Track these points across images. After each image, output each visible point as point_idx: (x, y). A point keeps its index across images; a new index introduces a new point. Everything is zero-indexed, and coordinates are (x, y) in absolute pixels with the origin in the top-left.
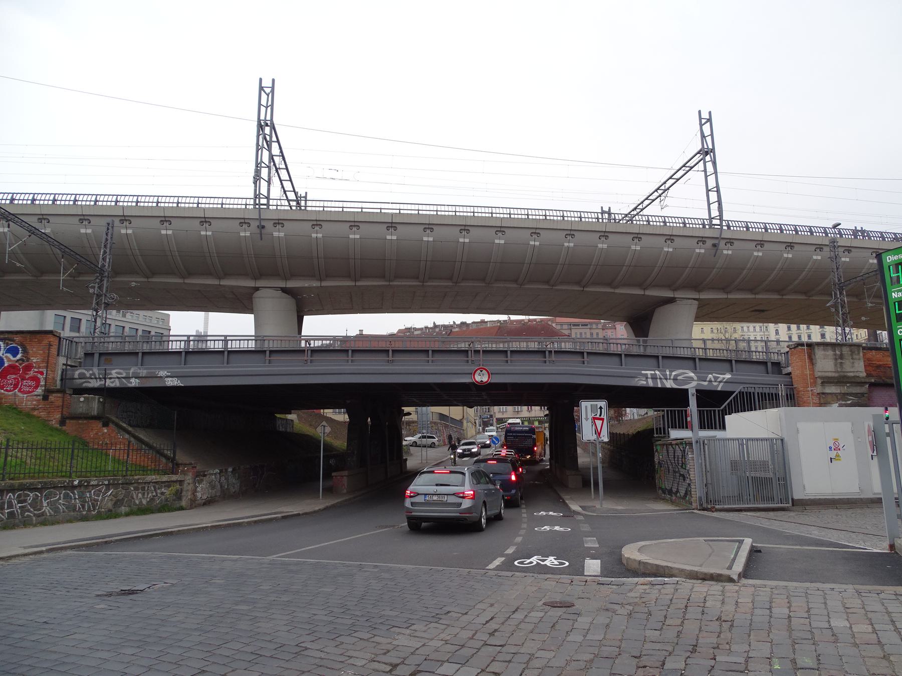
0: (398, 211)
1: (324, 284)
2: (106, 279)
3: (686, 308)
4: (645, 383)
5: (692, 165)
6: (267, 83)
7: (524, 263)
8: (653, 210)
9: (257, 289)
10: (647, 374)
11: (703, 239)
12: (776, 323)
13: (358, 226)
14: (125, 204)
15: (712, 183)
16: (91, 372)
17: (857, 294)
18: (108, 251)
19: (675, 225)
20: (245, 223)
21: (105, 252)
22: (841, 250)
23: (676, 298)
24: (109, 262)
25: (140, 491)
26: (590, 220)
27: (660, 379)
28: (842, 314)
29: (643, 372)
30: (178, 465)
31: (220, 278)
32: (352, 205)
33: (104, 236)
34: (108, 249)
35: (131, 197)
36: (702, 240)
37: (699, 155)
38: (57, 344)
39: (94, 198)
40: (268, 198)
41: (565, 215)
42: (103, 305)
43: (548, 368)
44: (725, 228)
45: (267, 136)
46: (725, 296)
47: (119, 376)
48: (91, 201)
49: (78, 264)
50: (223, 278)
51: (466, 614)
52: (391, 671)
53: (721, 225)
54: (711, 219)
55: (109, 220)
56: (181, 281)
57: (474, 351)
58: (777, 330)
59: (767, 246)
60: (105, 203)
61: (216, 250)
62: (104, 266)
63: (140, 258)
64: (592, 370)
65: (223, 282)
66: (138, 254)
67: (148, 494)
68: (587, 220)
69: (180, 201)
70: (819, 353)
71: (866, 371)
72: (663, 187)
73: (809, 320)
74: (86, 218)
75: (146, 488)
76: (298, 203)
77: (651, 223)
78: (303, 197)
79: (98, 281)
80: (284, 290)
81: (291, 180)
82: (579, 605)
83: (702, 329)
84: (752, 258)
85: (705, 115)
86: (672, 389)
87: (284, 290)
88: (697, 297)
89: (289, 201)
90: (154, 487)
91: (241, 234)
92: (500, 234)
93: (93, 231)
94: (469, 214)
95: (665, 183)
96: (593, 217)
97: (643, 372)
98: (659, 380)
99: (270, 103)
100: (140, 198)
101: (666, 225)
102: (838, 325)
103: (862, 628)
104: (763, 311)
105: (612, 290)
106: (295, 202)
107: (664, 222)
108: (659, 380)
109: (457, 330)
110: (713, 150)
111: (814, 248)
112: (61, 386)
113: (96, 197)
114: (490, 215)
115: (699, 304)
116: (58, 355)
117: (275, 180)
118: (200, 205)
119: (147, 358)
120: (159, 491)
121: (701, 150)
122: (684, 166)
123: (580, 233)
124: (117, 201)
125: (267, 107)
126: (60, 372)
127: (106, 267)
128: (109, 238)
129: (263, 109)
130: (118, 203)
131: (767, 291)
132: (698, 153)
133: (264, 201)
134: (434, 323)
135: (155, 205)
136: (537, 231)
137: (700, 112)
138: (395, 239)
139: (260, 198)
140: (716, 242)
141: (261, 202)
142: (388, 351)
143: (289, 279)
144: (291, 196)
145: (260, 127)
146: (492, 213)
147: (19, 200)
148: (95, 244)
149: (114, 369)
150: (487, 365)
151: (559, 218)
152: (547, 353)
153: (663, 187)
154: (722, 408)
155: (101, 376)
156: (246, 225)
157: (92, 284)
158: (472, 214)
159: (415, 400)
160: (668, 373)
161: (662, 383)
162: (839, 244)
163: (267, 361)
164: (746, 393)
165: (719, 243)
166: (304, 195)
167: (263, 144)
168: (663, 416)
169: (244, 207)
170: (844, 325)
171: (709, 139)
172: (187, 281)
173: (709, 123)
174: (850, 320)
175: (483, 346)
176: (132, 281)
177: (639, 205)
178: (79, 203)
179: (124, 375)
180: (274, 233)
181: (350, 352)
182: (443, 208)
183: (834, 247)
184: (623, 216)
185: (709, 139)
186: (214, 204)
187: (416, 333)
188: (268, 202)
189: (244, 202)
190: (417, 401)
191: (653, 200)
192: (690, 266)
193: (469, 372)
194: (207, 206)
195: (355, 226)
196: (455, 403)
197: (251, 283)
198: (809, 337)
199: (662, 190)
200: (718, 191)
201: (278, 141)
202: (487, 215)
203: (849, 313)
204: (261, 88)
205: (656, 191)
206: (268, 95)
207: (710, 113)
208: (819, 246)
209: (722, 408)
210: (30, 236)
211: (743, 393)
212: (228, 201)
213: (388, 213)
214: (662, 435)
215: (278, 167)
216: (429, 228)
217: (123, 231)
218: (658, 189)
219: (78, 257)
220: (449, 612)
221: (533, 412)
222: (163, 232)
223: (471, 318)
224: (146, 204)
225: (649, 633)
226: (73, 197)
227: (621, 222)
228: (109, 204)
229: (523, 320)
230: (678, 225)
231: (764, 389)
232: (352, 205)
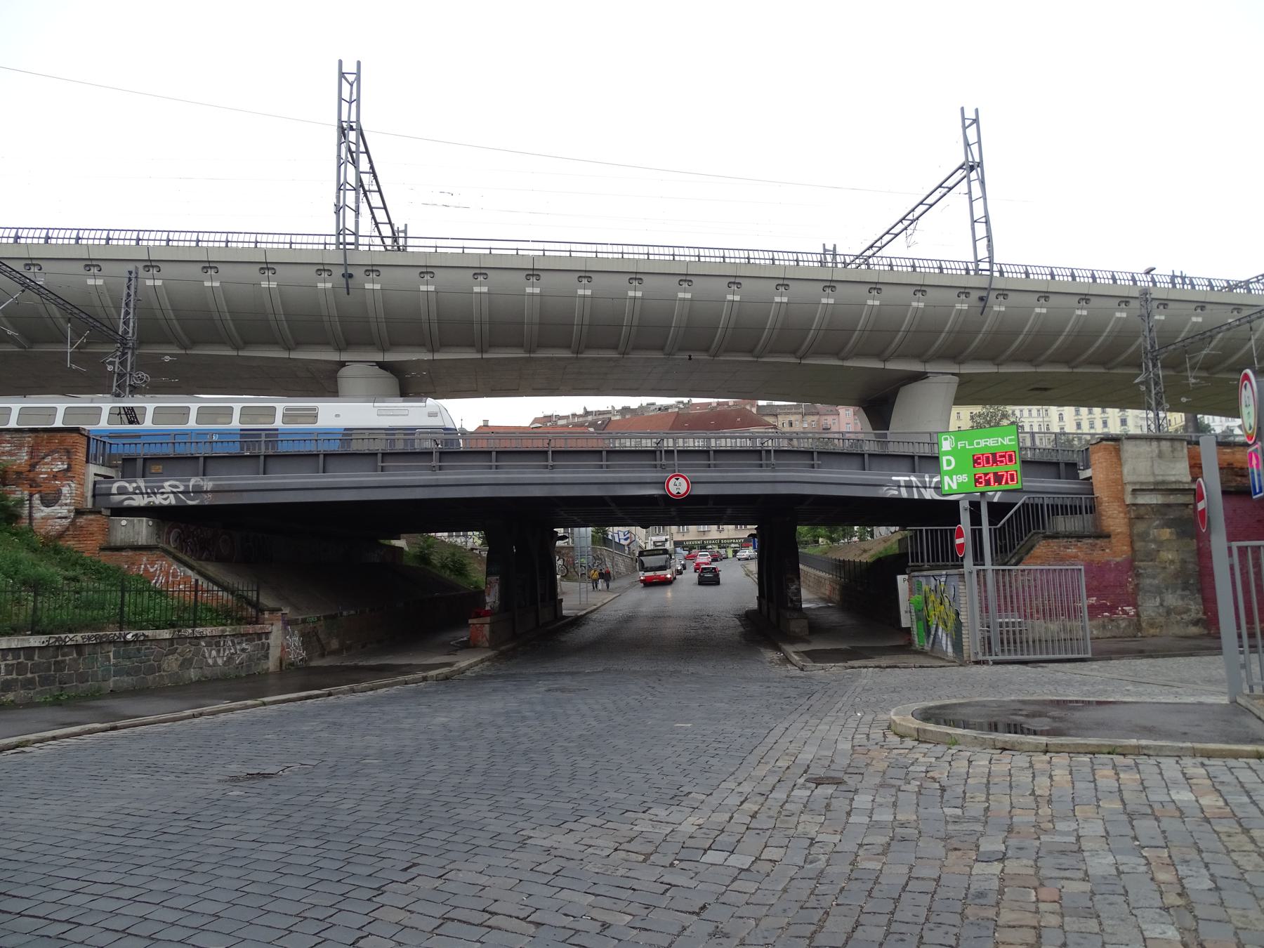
0: (541, 253)
1: (437, 356)
3: (941, 384)
4: (896, 493)
5: (951, 185)
6: (349, 67)
8: (897, 250)
9: (343, 364)
10: (899, 481)
11: (967, 291)
13: (432, 273)
15: (979, 213)
16: (135, 485)
17: (1175, 365)
20: (324, 270)
21: (127, 313)
22: (1155, 304)
25: (214, 647)
26: (811, 264)
27: (917, 487)
29: (894, 478)
30: (262, 611)
31: (289, 349)
33: (125, 291)
35: (159, 233)
36: (965, 291)
37: (961, 171)
38: (86, 447)
40: (355, 234)
42: (128, 389)
43: (559, 476)
44: (996, 274)
45: (351, 145)
46: (1033, 370)
47: (175, 490)
48: (39, 238)
49: (90, 330)
51: (711, 794)
52: (645, 861)
53: (991, 270)
54: (977, 261)
55: (131, 267)
57: (552, 452)
58: (1061, 414)
59: (1095, 302)
60: (121, 242)
61: (113, 303)
62: (126, 332)
63: (231, 322)
64: (781, 475)
65: (294, 355)
66: (173, 317)
68: (806, 264)
70: (1128, 448)
71: (1191, 473)
72: (910, 217)
73: (1105, 402)
75: (222, 643)
77: (895, 268)
79: (119, 353)
81: (385, 208)
82: (852, 782)
83: (958, 413)
84: (1033, 317)
85: (970, 114)
87: (382, 365)
88: (957, 371)
95: (913, 210)
97: (894, 478)
99: (354, 97)
100: (81, 232)
101: (915, 270)
102: (1149, 408)
103: (1210, 801)
104: (1045, 389)
105: (839, 363)
108: (915, 489)
109: (618, 418)
110: (980, 164)
111: (1193, 306)
113: (108, 234)
114: (671, 258)
116: (87, 462)
117: (364, 208)
118: (258, 245)
119: (330, 461)
120: (238, 647)
121: (964, 164)
122: (940, 186)
123: (747, 280)
124: (138, 240)
125: (350, 103)
126: (91, 486)
127: (130, 335)
128: (132, 293)
129: (345, 106)
130: (140, 242)
131: (1053, 361)
132: (961, 168)
133: (350, 239)
134: (585, 408)
135: (223, 245)
136: (738, 280)
137: (962, 109)
138: (379, 288)
139: (345, 235)
140: (984, 294)
141: (347, 241)
144: (386, 230)
145: (342, 132)
149: (167, 480)
151: (767, 262)
152: (764, 453)
153: (910, 217)
154: (999, 526)
155: (149, 491)
156: (326, 273)
157: (111, 359)
158: (646, 257)
159: (575, 518)
160: (927, 479)
161: (919, 492)
162: (1153, 296)
164: (1032, 505)
165: (988, 295)
166: (403, 228)
169: (322, 247)
170: (1157, 409)
171: (975, 148)
173: (975, 125)
174: (1166, 402)
178: (84, 242)
179: (182, 489)
183: (1147, 300)
184: (852, 258)
185: (975, 148)
186: (208, 241)
187: (561, 422)
188: (357, 240)
189: (322, 239)
190: (579, 520)
191: (897, 235)
193: (660, 481)
194: (269, 246)
196: (630, 522)
197: (334, 356)
199: (909, 220)
200: (987, 222)
201: (367, 152)
203: (1164, 392)
204: (342, 75)
205: (901, 221)
206: (351, 85)
207: (977, 111)
208: (1043, 295)
209: (999, 526)
210: (23, 291)
211: (1028, 504)
212: (299, 239)
213: (528, 256)
215: (367, 188)
217: (149, 283)
218: (904, 219)
220: (690, 793)
221: (726, 531)
223: (634, 402)
224: (181, 244)
225: (948, 811)
227: (849, 267)
228: (127, 243)
230: (932, 270)
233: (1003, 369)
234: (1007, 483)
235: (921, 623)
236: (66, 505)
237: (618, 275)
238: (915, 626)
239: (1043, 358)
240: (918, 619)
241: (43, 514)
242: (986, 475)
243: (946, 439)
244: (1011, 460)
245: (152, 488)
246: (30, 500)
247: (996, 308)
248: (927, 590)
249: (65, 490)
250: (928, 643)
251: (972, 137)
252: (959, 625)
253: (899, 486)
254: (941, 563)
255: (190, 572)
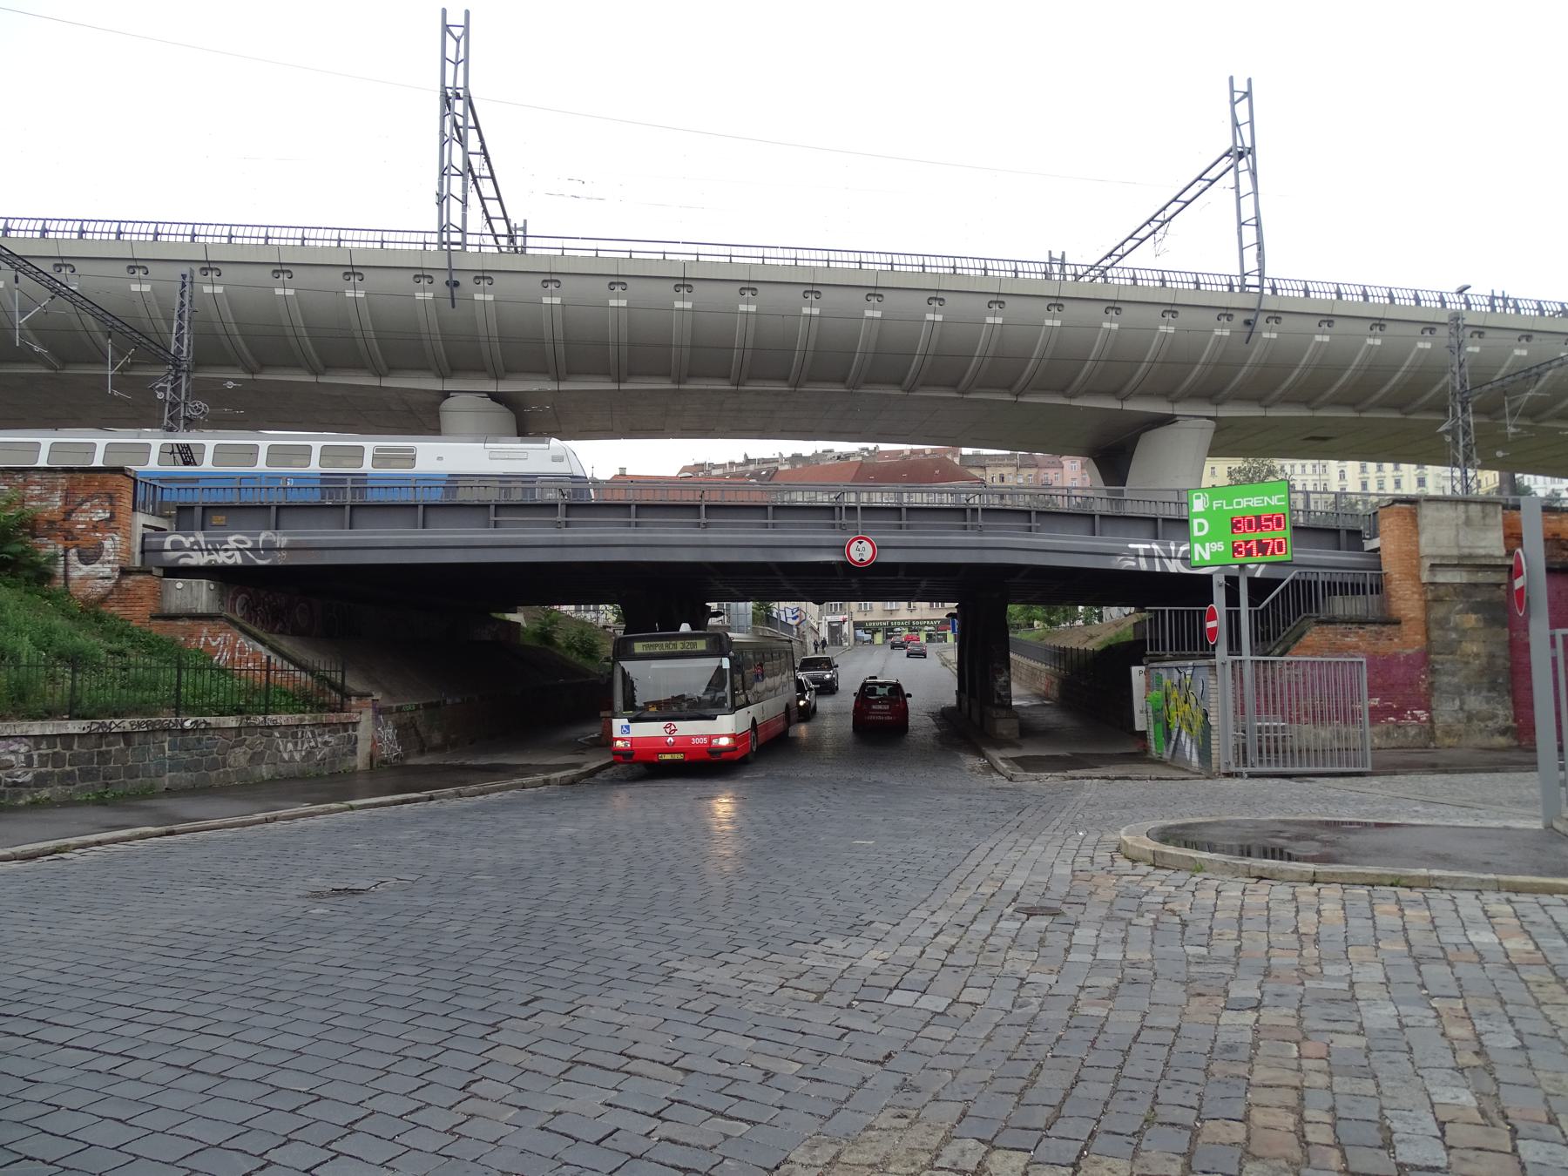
1: (564, 386)
2: (184, 376)
4: (1133, 564)
6: (455, 18)
7: (855, 353)
8: (1143, 259)
9: (446, 395)
10: (1137, 550)
12: (1342, 459)
13: (558, 281)
14: (209, 240)
16: (192, 539)
17: (1490, 410)
18: (186, 324)
19: (1180, 286)
21: (181, 327)
22: (1468, 332)
23: (1176, 416)
24: (189, 345)
26: (1033, 276)
27: (1160, 557)
28: (1464, 446)
29: (1131, 546)
31: (381, 375)
32: (747, 251)
33: (178, 300)
34: (186, 322)
36: (1226, 313)
37: (1226, 159)
39: (152, 229)
40: (462, 231)
41: (989, 266)
42: (182, 422)
44: (1268, 292)
47: (241, 546)
50: (386, 376)
53: (1261, 286)
54: (1244, 275)
55: (185, 269)
56: (312, 379)
60: (172, 239)
61: (234, 317)
63: (239, 339)
65: (388, 382)
66: (305, 334)
67: (303, 744)
68: (1027, 276)
69: (270, 235)
70: (1428, 513)
72: (1160, 217)
74: (139, 264)
75: (300, 734)
76: (512, 238)
78: (520, 229)
79: (171, 378)
80: (495, 397)
83: (1213, 468)
84: (1312, 346)
85: (1241, 86)
86: (1179, 575)
88: (1213, 414)
89: (496, 237)
90: (313, 732)
91: (348, 295)
92: (874, 300)
93: (152, 288)
94: (820, 264)
96: (1008, 268)
97: (1131, 546)
98: (1157, 560)
99: (461, 56)
102: (1455, 465)
105: (1066, 402)
106: (506, 239)
107: (1195, 283)
108: (1157, 560)
109: (787, 467)
110: (1251, 151)
112: (143, 561)
115: (1217, 426)
116: (134, 509)
117: (473, 198)
121: (1231, 150)
122: (1200, 178)
125: (456, 64)
126: (139, 540)
127: (185, 354)
129: (450, 67)
130: (196, 238)
131: (1336, 403)
132: (1227, 154)
133: (456, 237)
134: (746, 455)
137: (1231, 79)
139: (449, 232)
140: (1251, 316)
141: (452, 240)
142: (698, 507)
143: (503, 379)
144: (501, 227)
145: (447, 102)
146: (860, 262)
147: (94, 232)
148: (158, 310)
149: (232, 534)
150: (870, 533)
151: (978, 272)
152: (969, 512)
153: (1160, 217)
154: (1261, 607)
156: (426, 280)
159: (732, 589)
160: (1173, 548)
161: (1162, 564)
162: (1466, 322)
163: (492, 524)
164: (1303, 582)
165: (1256, 318)
167: (452, 134)
168: (1150, 620)
169: (421, 247)
170: (1465, 465)
171: (1245, 130)
172: (322, 379)
173: (1246, 100)
175: (864, 497)
176: (229, 379)
177: (1117, 248)
178: (127, 237)
179: (249, 545)
180: (416, 294)
181: (633, 508)
182: (773, 253)
184: (1085, 269)
185: (1245, 130)
187: (715, 472)
188: (464, 238)
189: (421, 238)
191: (1142, 240)
192: (1091, 358)
194: (356, 245)
195: (552, 281)
197: (435, 385)
198: (1398, 484)
199: (1159, 221)
200: (1258, 225)
201: (477, 127)
202: (852, 266)
204: (446, 28)
206: (458, 41)
209: (1261, 607)
210: (53, 298)
211: (1298, 581)
214: (1161, 652)
215: (477, 174)
216: (749, 289)
217: (207, 289)
219: (136, 335)
222: (279, 292)
223: (807, 448)
224: (246, 241)
226: (153, 226)
227: (1081, 280)
228: (180, 239)
229: (902, 451)
230: (1186, 286)
231: (1309, 575)
232: (747, 251)
233: (1272, 413)
234: (1273, 553)
235: (1160, 726)
236: (109, 562)
237: (779, 286)
238: (1152, 730)
239: (1322, 398)
240: (1157, 721)
241: (81, 573)
242: (1247, 542)
243: (1198, 497)
244: (1279, 525)
245: (213, 543)
246: (65, 556)
247: (1266, 335)
248: (1169, 684)
249: (108, 544)
250: (1168, 750)
251: (1243, 116)
252: (1207, 728)
253: (1138, 556)
254: (1187, 652)
255: (260, 648)
